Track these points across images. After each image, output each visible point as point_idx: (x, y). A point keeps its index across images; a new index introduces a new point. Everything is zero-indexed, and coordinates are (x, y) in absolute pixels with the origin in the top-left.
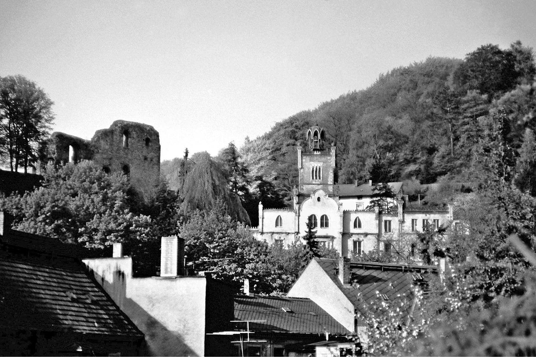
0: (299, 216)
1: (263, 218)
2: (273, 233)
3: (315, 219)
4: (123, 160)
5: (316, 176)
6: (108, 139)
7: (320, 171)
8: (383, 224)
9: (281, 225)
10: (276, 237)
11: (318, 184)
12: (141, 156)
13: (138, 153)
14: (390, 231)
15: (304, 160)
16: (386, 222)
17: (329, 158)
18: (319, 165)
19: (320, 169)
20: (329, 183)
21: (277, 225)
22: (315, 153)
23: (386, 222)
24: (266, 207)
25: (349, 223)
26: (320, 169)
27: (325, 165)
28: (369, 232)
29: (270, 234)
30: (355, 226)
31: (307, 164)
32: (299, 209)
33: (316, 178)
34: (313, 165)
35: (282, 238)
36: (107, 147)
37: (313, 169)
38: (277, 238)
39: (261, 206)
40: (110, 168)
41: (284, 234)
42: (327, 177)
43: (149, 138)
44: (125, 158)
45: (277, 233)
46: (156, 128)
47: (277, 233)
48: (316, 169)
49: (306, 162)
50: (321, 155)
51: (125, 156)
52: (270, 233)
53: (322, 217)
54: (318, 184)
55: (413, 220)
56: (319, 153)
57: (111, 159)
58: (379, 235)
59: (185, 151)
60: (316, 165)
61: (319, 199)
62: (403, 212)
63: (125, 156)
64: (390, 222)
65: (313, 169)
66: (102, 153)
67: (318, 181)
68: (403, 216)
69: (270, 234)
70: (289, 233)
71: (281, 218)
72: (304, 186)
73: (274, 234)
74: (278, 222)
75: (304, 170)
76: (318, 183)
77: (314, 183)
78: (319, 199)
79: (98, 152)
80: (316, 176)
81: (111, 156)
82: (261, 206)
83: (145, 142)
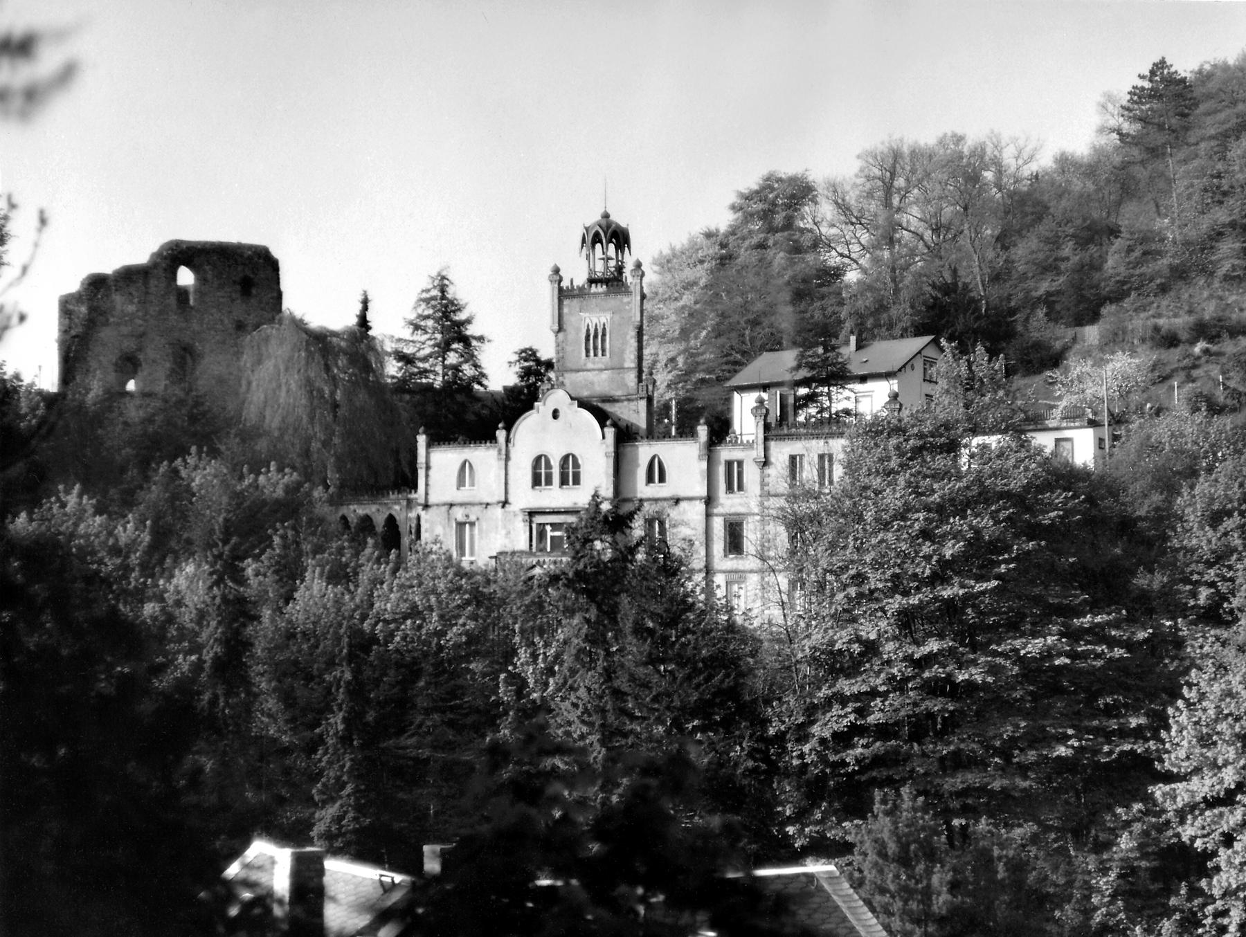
0: (507, 458)
1: (428, 468)
2: (451, 505)
3: (548, 466)
4: (176, 334)
5: (595, 348)
6: (132, 290)
7: (604, 335)
8: (721, 470)
9: (472, 484)
10: (459, 514)
11: (601, 370)
12: (226, 321)
13: (217, 316)
14: (740, 488)
15: (566, 310)
16: (729, 464)
17: (626, 299)
18: (603, 320)
19: (604, 329)
20: (626, 365)
21: (461, 482)
22: (594, 289)
23: (729, 464)
24: (439, 438)
25: (633, 474)
26: (604, 329)
27: (617, 317)
28: (682, 494)
29: (444, 509)
30: (650, 479)
31: (573, 319)
32: (508, 440)
33: (595, 355)
34: (588, 321)
35: (473, 518)
36: (131, 308)
37: (588, 330)
38: (460, 518)
39: (422, 440)
40: (141, 357)
41: (476, 508)
42: (622, 352)
43: (246, 275)
44: (181, 330)
45: (461, 505)
46: (276, 253)
47: (461, 505)
48: (596, 330)
49: (571, 314)
50: (607, 294)
51: (184, 325)
52: (444, 504)
53: (565, 459)
54: (601, 370)
55: (793, 458)
56: (601, 289)
57: (142, 335)
58: (709, 501)
59: (361, 298)
60: (595, 320)
61: (555, 414)
62: (766, 439)
63: (184, 325)
64: (740, 463)
65: (588, 330)
66: (118, 324)
67: (602, 361)
68: (766, 449)
69: (444, 509)
70: (488, 504)
71: (470, 465)
72: (566, 375)
73: (455, 509)
74: (464, 473)
75: (566, 336)
76: (601, 366)
77: (590, 366)
78: (555, 414)
79: (106, 323)
80: (595, 348)
81: (142, 329)
82: (422, 440)
83: (238, 287)
